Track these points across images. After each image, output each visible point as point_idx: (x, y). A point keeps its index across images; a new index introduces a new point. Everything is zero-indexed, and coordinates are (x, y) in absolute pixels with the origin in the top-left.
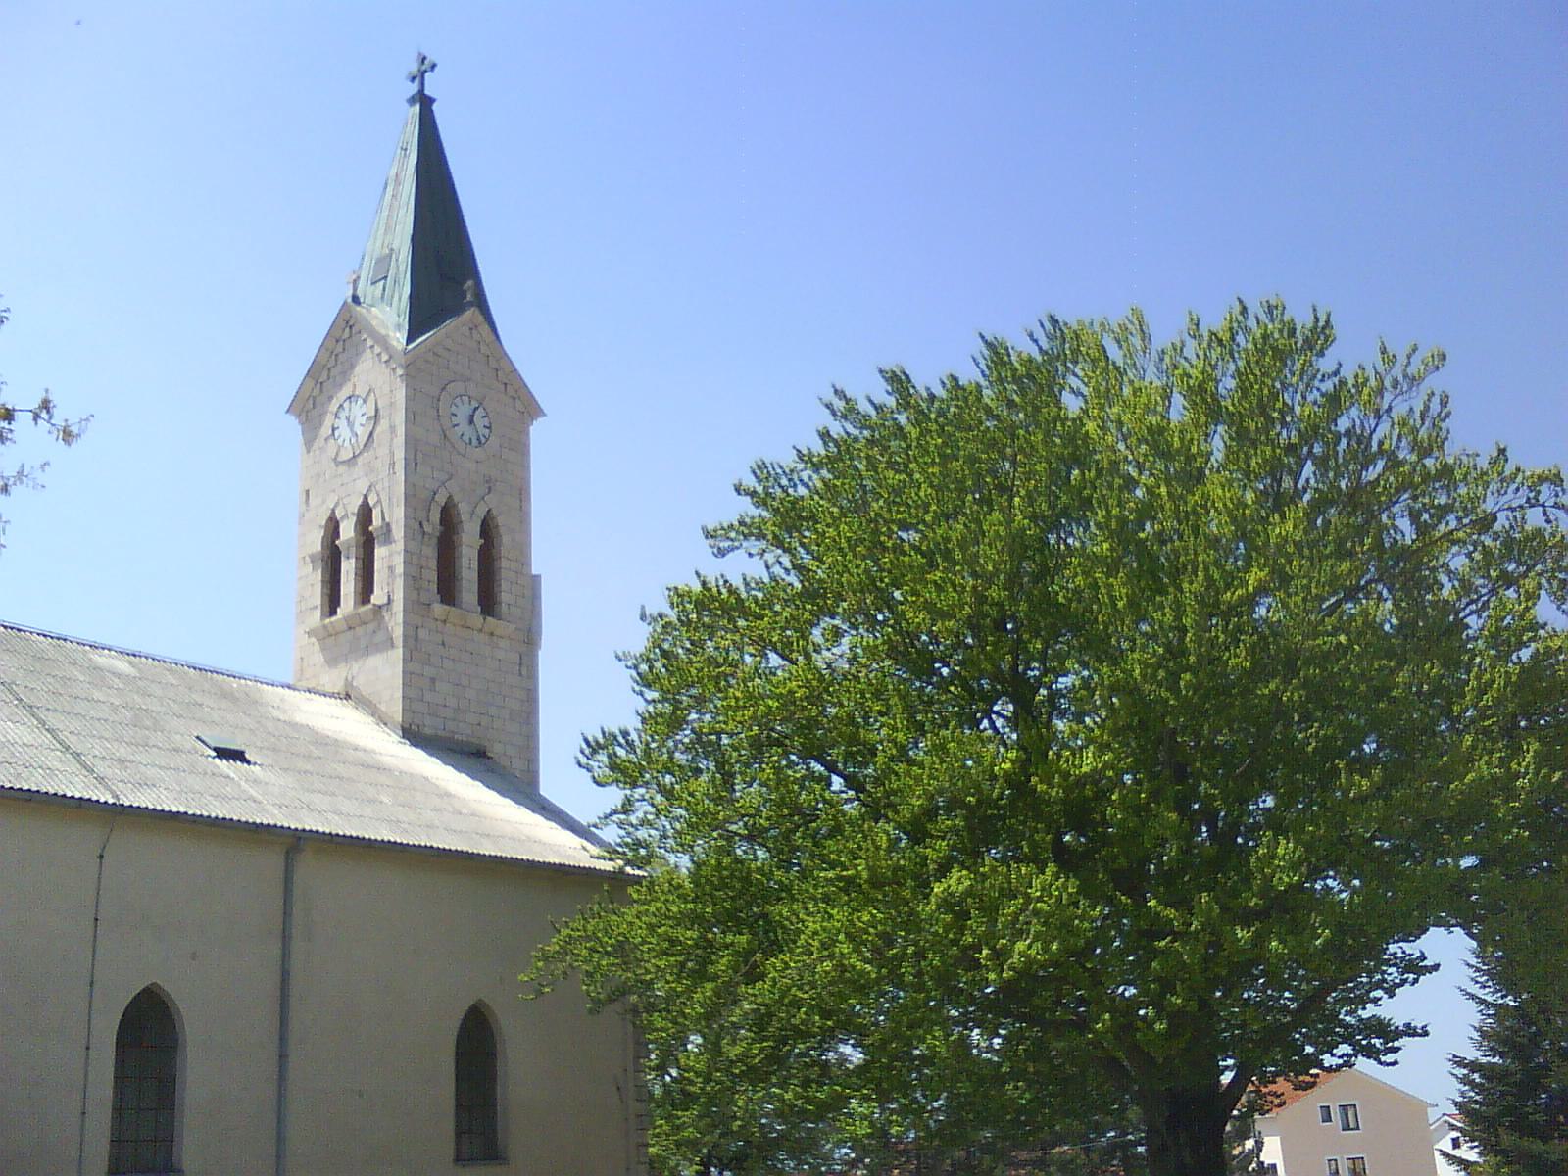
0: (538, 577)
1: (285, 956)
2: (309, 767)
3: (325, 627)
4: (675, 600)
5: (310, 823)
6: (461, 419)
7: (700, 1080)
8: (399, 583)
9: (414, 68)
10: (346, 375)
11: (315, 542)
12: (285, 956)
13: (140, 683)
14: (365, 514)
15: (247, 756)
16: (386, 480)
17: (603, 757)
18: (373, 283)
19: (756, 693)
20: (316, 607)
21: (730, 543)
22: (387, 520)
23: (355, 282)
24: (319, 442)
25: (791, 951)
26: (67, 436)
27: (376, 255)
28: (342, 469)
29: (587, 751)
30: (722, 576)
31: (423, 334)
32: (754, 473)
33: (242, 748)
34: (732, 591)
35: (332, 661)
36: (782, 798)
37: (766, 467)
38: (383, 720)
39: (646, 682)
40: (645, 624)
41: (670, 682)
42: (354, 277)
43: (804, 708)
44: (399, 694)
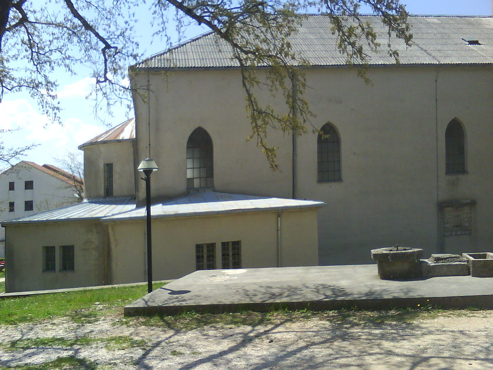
15: (479, 42)
33: (477, 40)
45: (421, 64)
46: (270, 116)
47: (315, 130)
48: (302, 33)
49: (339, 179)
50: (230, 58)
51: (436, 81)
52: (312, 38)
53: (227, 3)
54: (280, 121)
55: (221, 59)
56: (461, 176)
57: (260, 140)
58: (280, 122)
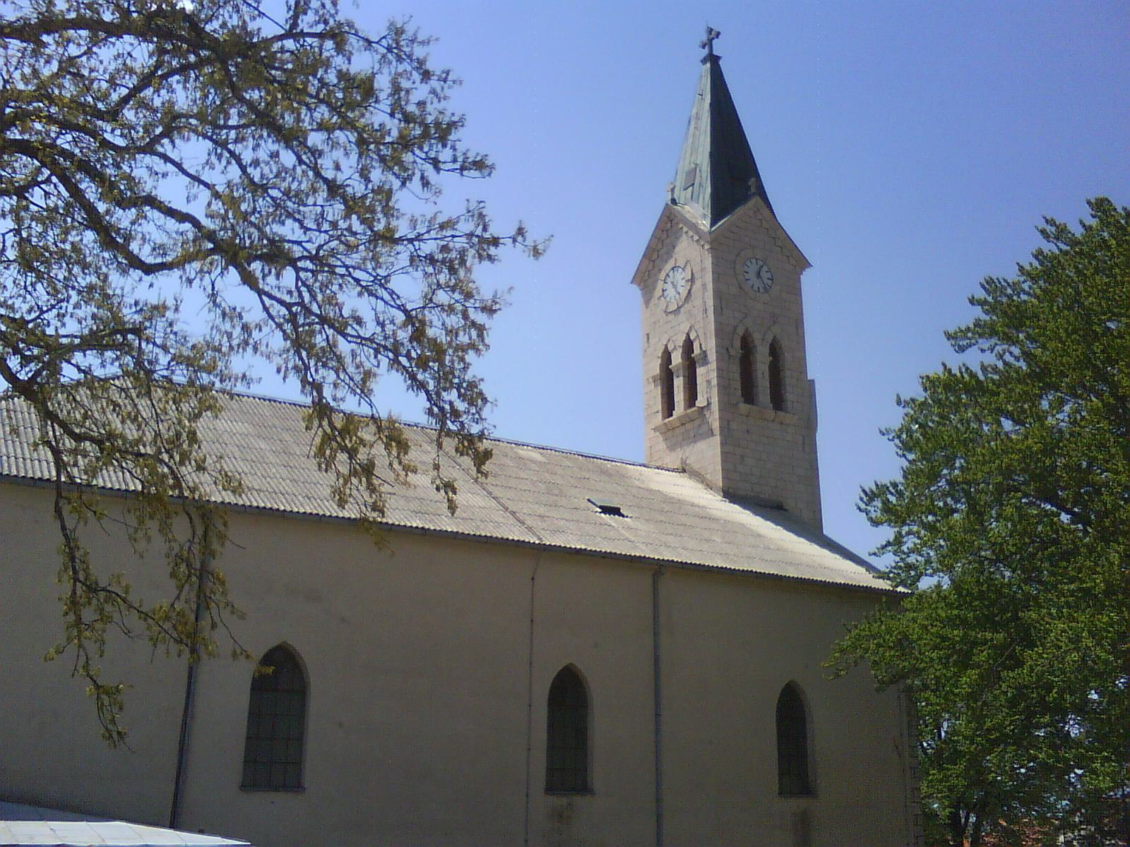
0: (813, 381)
1: (656, 647)
2: (663, 518)
3: (665, 424)
4: (928, 385)
5: (667, 556)
6: (752, 276)
7: (968, 742)
8: (715, 391)
9: (704, 38)
10: (669, 255)
11: (656, 368)
12: (656, 647)
13: (548, 466)
14: (688, 345)
15: (621, 511)
16: (701, 321)
17: (878, 503)
18: (685, 189)
19: (999, 451)
20: (658, 412)
21: (968, 341)
22: (704, 349)
23: (673, 190)
24: (654, 301)
25: (1042, 645)
26: (536, 252)
27: (686, 169)
28: (671, 317)
29: (865, 499)
30: (964, 365)
31: (723, 218)
32: (983, 286)
33: (619, 506)
34: (973, 375)
35: (672, 448)
36: (1025, 529)
37: (994, 282)
38: (709, 486)
39: (906, 447)
40: (901, 408)
41: (927, 446)
42: (672, 186)
43: (1039, 460)
44: (719, 467)
45: (502, 538)
46: (119, 600)
47: (238, 652)
48: (240, 435)
49: (296, 786)
50: (32, 441)
51: (533, 579)
52: (263, 447)
53: (52, 322)
54: (145, 616)
55: (24, 459)
56: (580, 801)
57: (82, 660)
58: (145, 620)
